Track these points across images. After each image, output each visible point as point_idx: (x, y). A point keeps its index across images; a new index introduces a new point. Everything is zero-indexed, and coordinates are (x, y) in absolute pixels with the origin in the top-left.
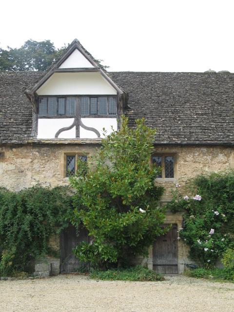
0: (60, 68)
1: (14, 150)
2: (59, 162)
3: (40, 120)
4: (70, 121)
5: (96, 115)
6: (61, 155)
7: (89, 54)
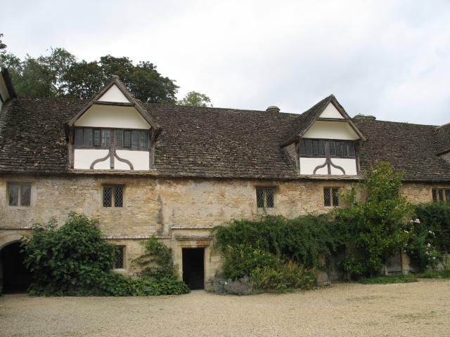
0: (125, 101)
1: (286, 183)
2: (319, 195)
3: (76, 150)
4: (105, 153)
5: (129, 148)
6: (321, 187)
7: (341, 107)
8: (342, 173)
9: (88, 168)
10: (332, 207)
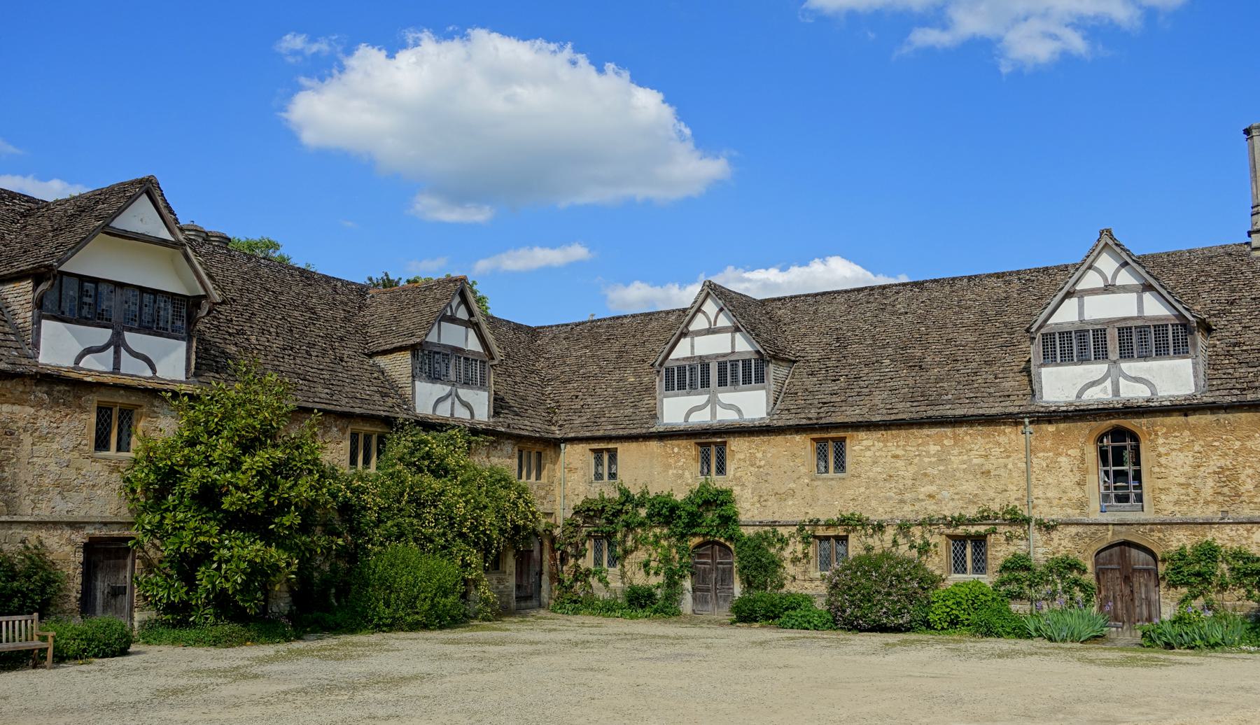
6: (93, 400)
8: (149, 373)
9: (70, 363)
10: (969, 577)
